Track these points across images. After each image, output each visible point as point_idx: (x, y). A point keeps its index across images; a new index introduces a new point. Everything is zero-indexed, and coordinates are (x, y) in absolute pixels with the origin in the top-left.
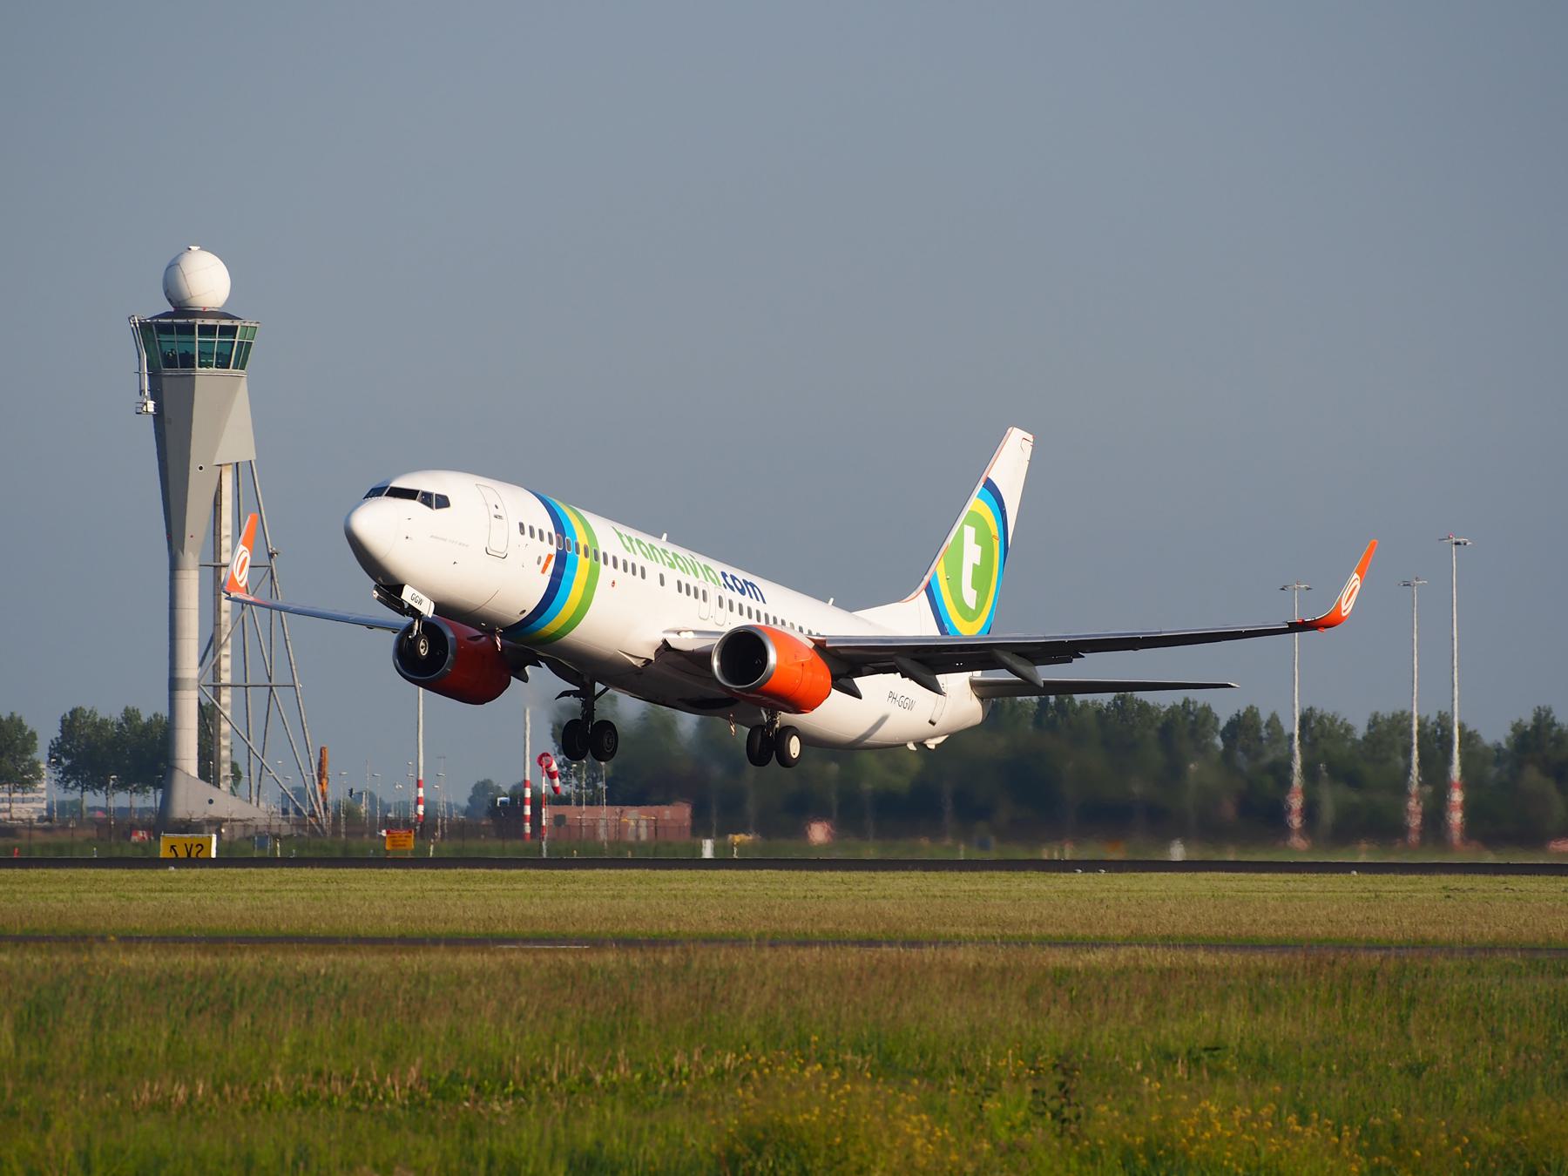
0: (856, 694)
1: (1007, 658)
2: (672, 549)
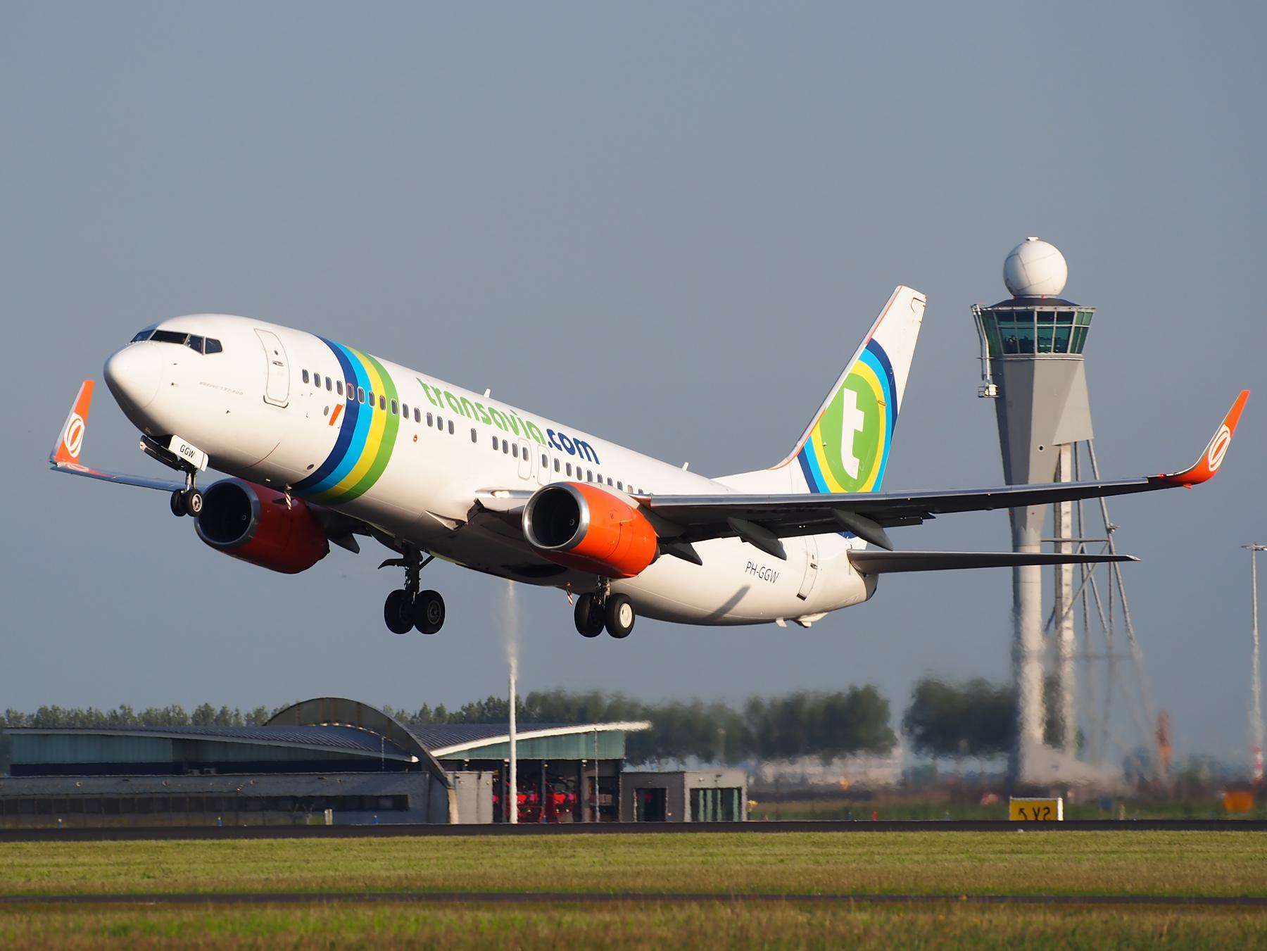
0: (696, 560)
1: (851, 519)
2: (501, 407)
